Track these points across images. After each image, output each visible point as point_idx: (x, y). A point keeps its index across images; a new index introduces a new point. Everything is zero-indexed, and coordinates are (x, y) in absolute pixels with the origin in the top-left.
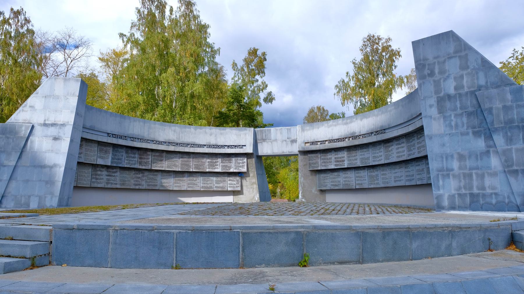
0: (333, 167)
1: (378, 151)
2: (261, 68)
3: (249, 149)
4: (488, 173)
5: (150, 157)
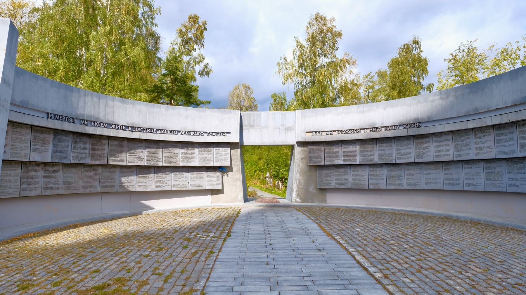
0: (340, 162)
1: (405, 147)
2: (199, 39)
3: (234, 138)
5: (106, 147)
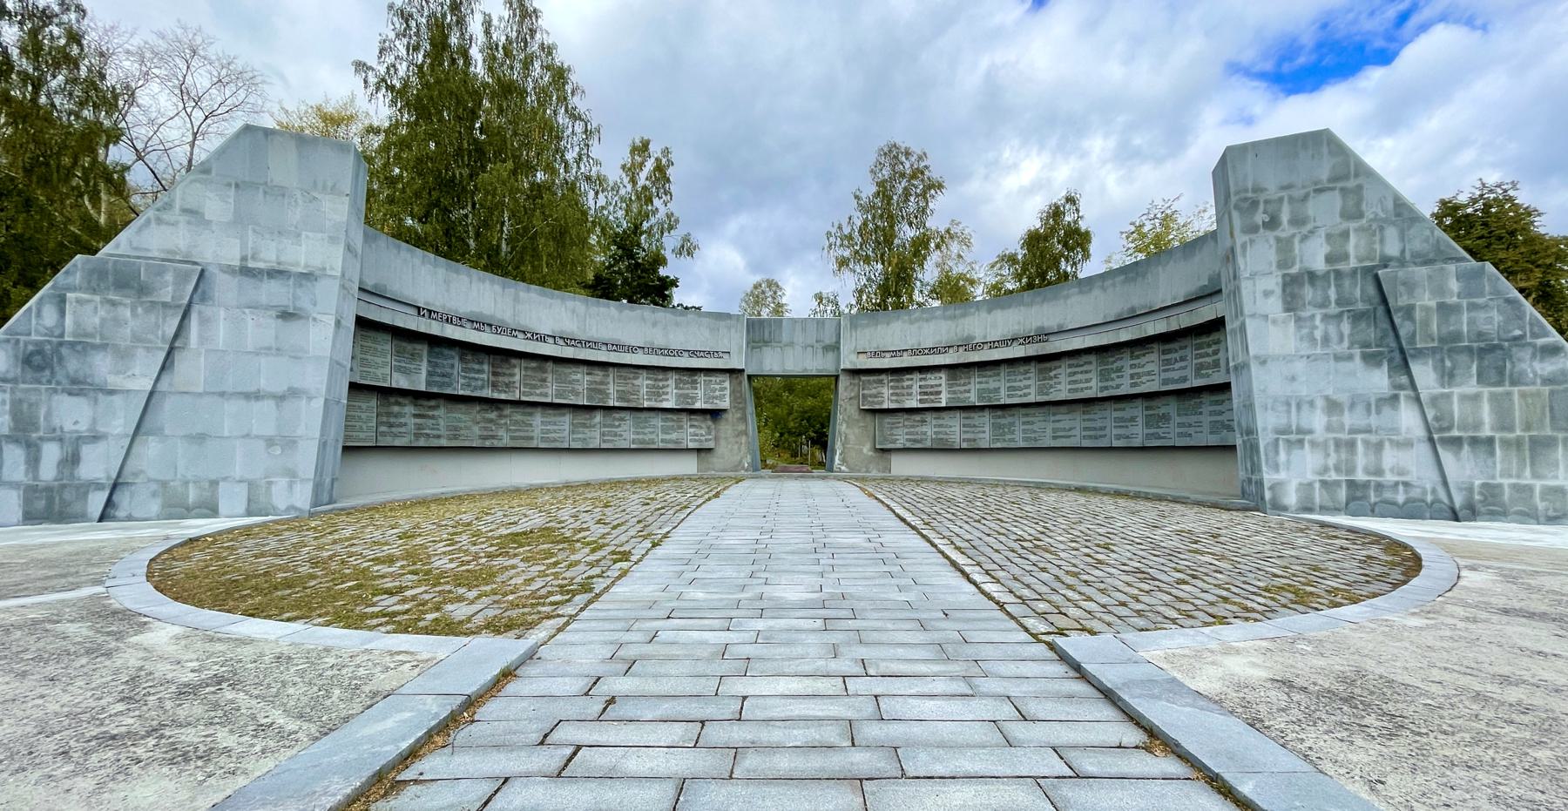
4: (1391, 441)
